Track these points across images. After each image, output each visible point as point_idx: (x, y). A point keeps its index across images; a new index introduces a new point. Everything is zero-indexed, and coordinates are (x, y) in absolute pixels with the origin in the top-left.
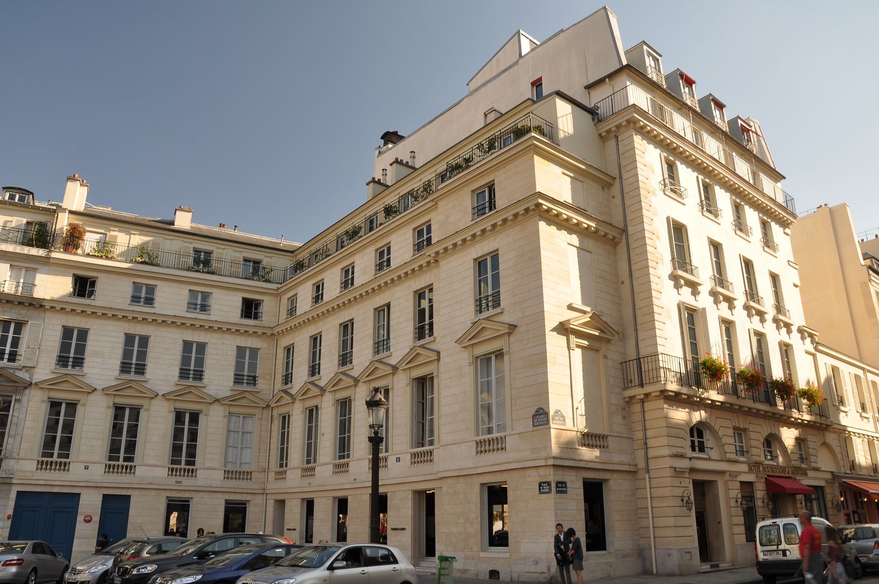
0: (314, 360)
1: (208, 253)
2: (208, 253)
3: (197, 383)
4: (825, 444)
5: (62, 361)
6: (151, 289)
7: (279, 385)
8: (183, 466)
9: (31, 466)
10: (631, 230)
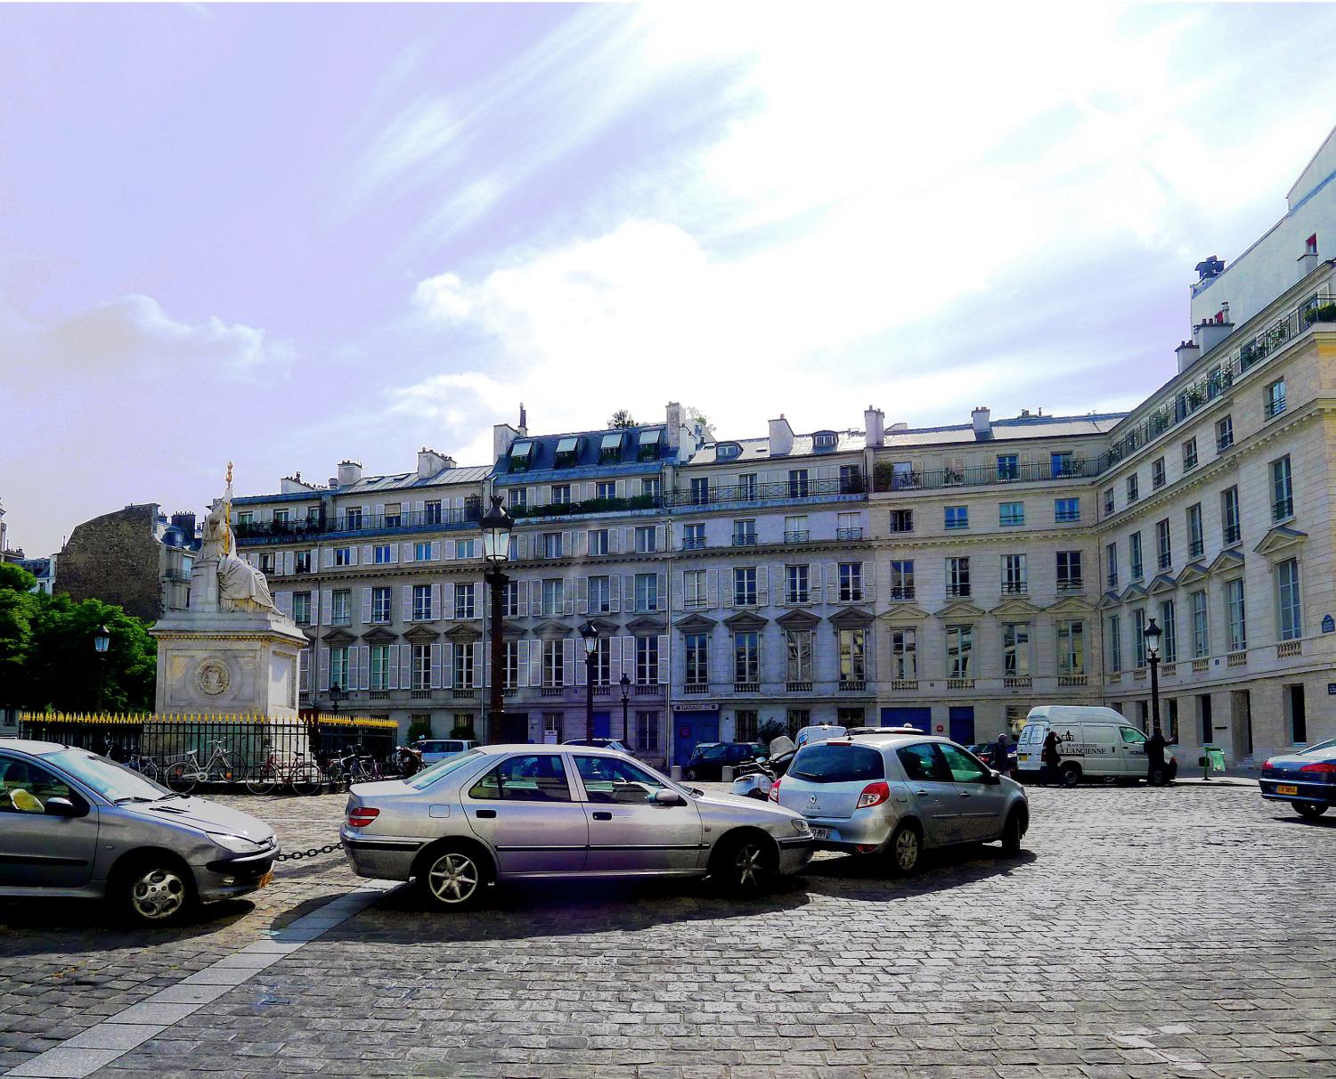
0: (1136, 561)
1: (1013, 457)
2: (1013, 457)
5: (896, 593)
6: (963, 511)
7: (1106, 588)
9: (887, 687)
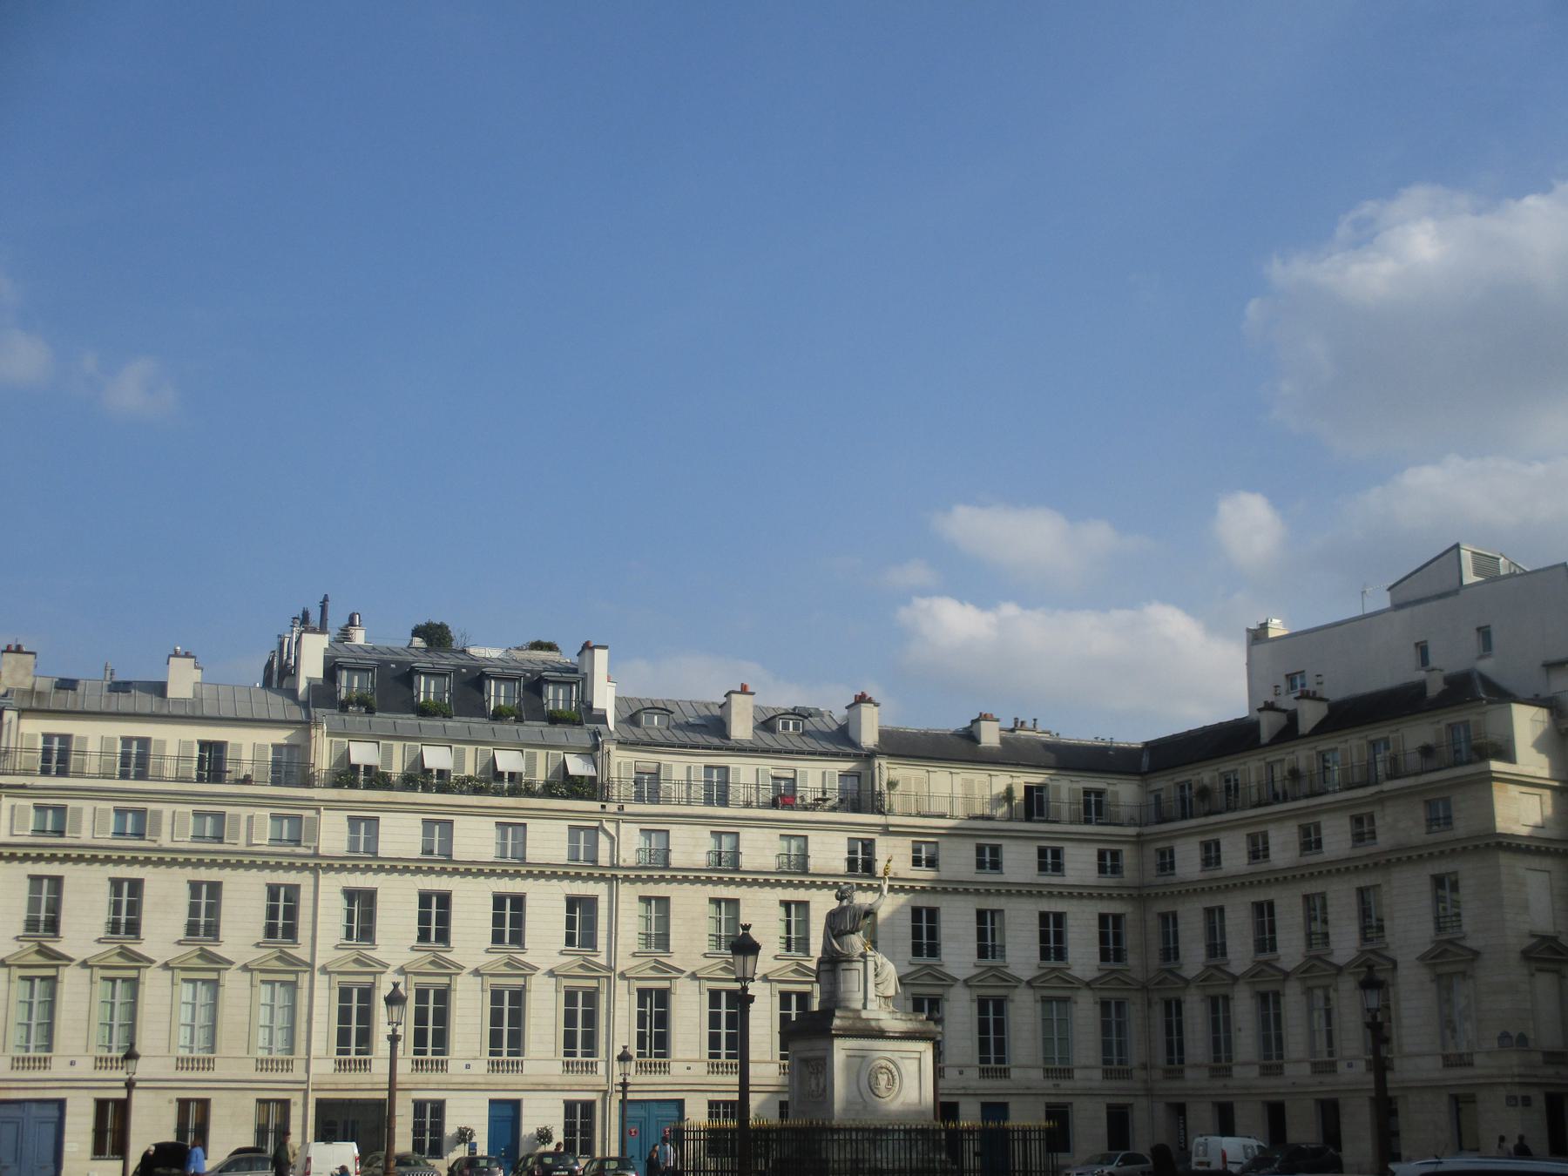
3: (932, 961)
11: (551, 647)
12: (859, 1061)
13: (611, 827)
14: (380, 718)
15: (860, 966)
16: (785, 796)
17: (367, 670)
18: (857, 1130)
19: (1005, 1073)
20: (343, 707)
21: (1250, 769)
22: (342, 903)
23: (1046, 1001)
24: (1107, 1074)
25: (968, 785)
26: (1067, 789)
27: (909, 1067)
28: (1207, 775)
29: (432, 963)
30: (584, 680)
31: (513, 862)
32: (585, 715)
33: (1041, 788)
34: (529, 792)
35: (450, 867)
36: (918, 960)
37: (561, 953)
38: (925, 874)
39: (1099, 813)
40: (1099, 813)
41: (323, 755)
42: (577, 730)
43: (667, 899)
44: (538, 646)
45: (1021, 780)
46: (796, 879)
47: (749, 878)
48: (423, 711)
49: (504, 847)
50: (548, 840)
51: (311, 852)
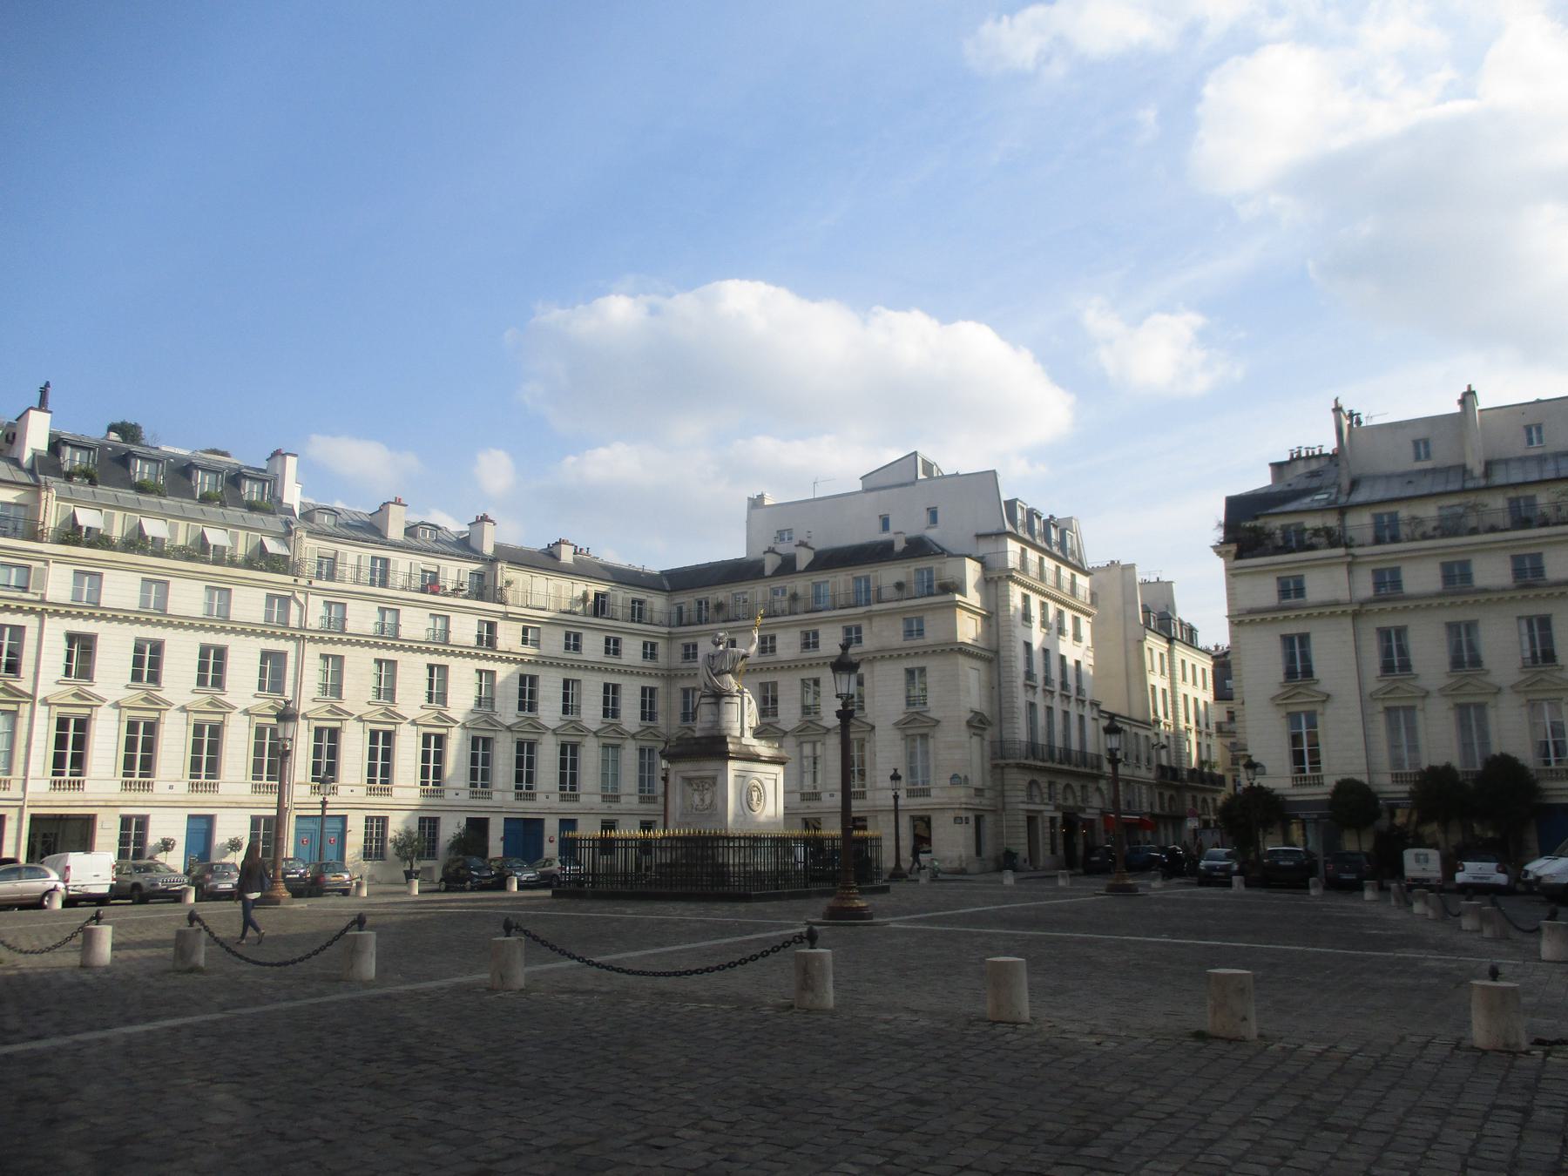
3: (531, 715)
4: (1098, 789)
8: (137, 778)
10: (1002, 653)
11: (225, 454)
12: (742, 776)
13: (301, 597)
14: (100, 489)
15: (738, 700)
16: (431, 584)
17: (89, 449)
18: (745, 838)
19: (576, 798)
20: (69, 477)
21: (757, 592)
22: (63, 645)
23: (605, 746)
24: (642, 800)
25: (558, 588)
26: (621, 597)
27: (769, 786)
28: (721, 594)
29: (144, 699)
30: (276, 480)
31: (219, 619)
32: (271, 505)
33: (604, 595)
34: (233, 563)
35: (165, 620)
36: (522, 714)
37: (255, 696)
38: (530, 650)
39: (640, 615)
40: (640, 615)
41: (52, 513)
42: (271, 518)
43: (342, 657)
44: (215, 452)
45: (594, 588)
46: (441, 648)
47: (407, 645)
48: (141, 488)
49: (210, 606)
50: (249, 603)
51: (38, 598)
